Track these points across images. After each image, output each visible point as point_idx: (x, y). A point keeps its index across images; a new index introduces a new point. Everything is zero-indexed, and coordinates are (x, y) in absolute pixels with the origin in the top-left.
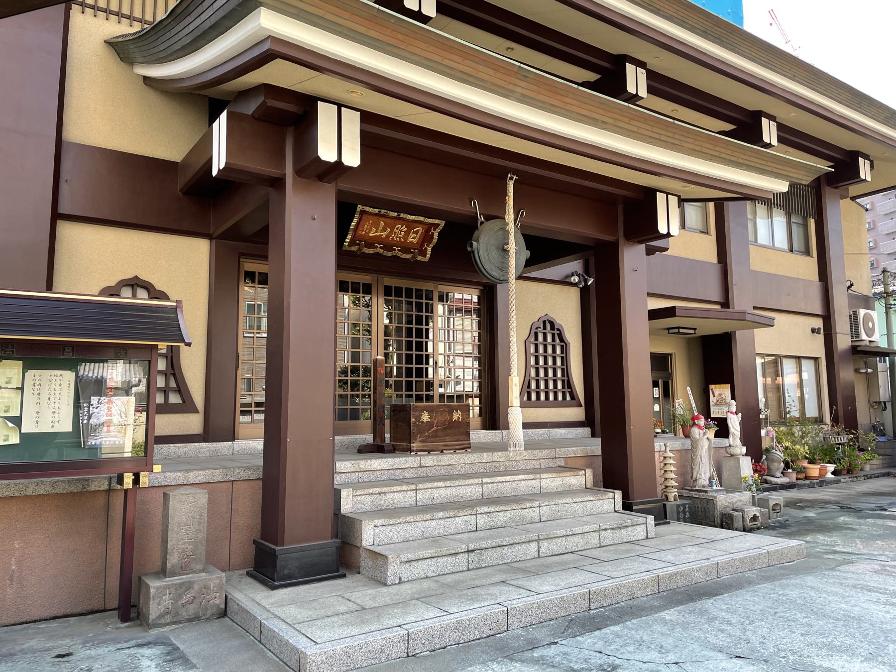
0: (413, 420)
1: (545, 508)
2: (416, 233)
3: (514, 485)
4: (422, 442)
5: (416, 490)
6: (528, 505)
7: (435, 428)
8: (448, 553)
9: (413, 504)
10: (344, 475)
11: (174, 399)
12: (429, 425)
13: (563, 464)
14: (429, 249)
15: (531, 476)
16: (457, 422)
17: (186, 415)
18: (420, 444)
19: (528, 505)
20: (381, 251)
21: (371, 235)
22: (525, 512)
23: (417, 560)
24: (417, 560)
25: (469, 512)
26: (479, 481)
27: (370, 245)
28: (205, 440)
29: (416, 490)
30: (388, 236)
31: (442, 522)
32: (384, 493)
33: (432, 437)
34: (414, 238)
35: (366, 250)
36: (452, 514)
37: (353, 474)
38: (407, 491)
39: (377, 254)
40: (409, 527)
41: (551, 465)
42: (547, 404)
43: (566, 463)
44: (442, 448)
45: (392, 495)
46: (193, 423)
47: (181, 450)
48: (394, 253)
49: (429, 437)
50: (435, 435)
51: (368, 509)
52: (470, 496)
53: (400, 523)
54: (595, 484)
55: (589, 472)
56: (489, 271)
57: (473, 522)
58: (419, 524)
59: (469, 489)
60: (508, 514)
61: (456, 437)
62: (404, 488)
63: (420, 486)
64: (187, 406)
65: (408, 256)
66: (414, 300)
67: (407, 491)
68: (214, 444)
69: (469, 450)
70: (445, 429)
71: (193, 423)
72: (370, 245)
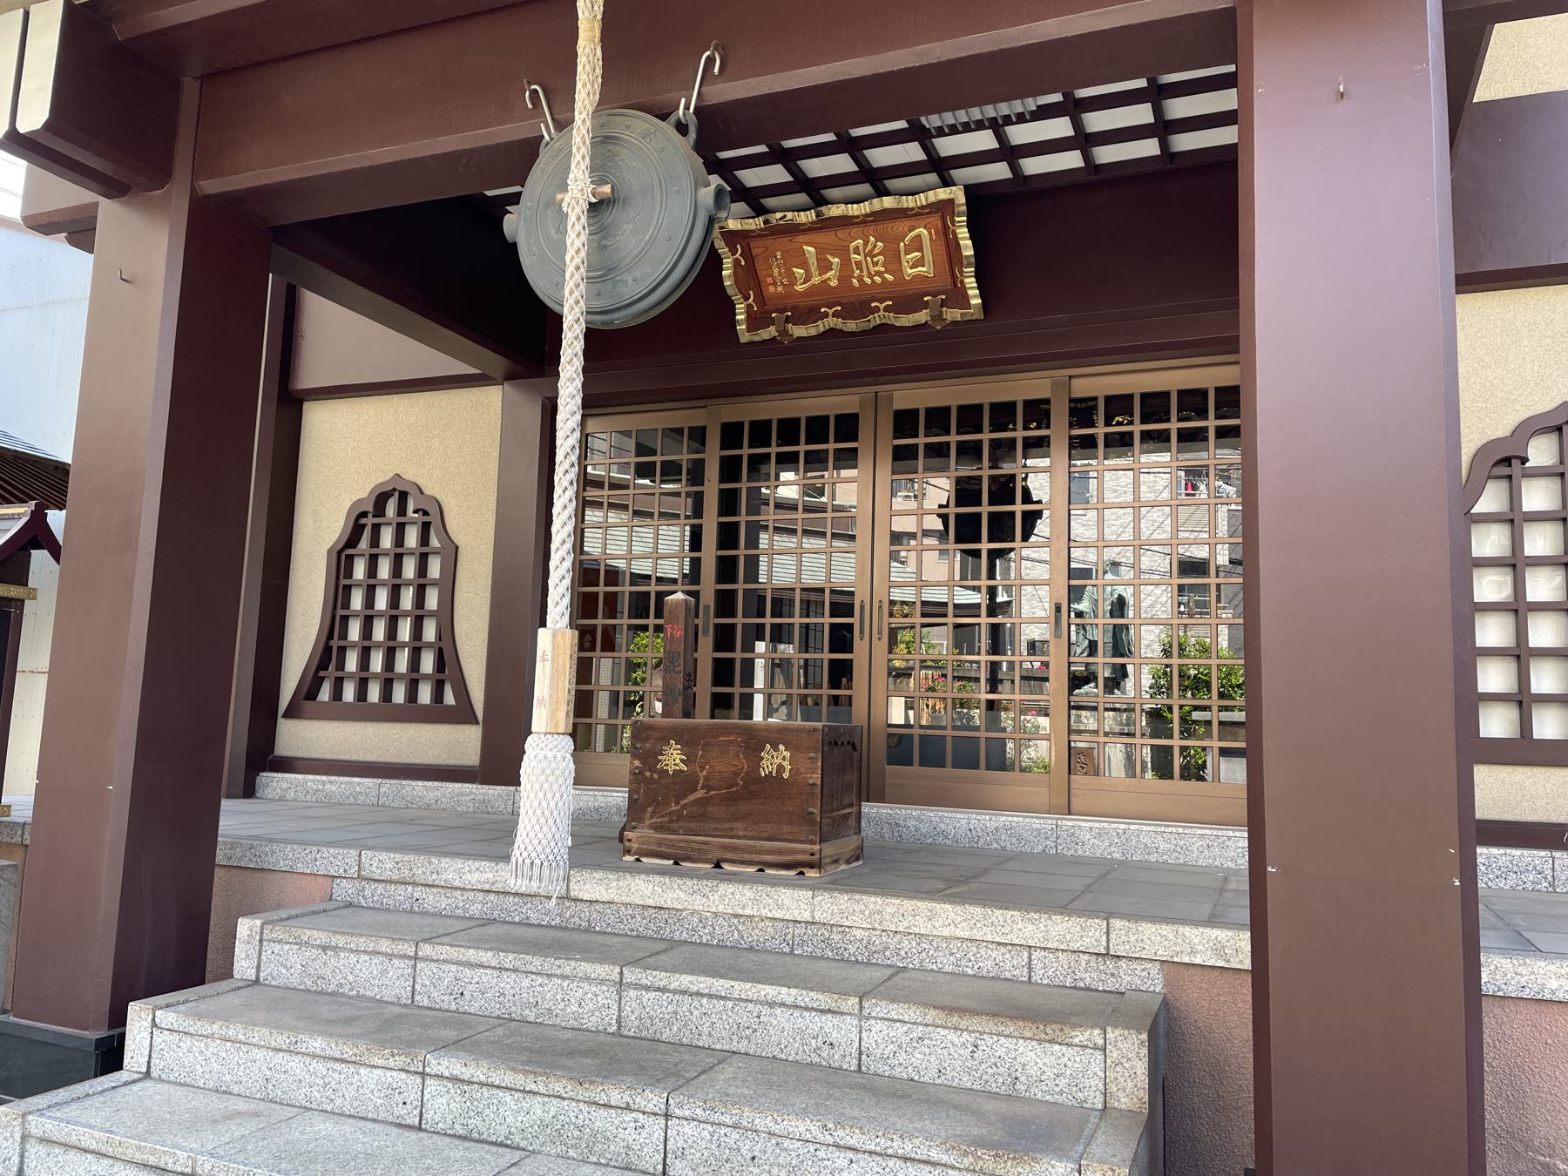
1: (688, 1128)
2: (917, 244)
3: (744, 1015)
4: (658, 828)
5: (416, 958)
6: (616, 1097)
7: (700, 794)
8: (138, 1157)
12: (685, 783)
14: (971, 282)
15: (823, 1000)
16: (775, 780)
18: (651, 834)
19: (616, 1097)
20: (838, 323)
21: (799, 288)
22: (602, 1120)
23: (67, 1146)
24: (67, 1146)
25: (400, 1061)
26: (610, 971)
27: (808, 314)
30: (845, 278)
31: (321, 1067)
32: (335, 949)
33: (692, 817)
35: (799, 331)
36: (348, 1052)
38: (391, 956)
39: (831, 332)
40: (235, 1056)
42: (387, 712)
44: (719, 855)
48: (737, 298)
49: (680, 817)
50: (699, 816)
51: (295, 981)
53: (211, 1036)
57: (413, 1096)
58: (259, 1055)
59: (578, 991)
60: (537, 1107)
61: (768, 828)
62: (385, 945)
63: (426, 950)
64: (462, 713)
65: (922, 316)
67: (391, 956)
69: (811, 874)
70: (732, 799)
71: (464, 744)
72: (808, 314)
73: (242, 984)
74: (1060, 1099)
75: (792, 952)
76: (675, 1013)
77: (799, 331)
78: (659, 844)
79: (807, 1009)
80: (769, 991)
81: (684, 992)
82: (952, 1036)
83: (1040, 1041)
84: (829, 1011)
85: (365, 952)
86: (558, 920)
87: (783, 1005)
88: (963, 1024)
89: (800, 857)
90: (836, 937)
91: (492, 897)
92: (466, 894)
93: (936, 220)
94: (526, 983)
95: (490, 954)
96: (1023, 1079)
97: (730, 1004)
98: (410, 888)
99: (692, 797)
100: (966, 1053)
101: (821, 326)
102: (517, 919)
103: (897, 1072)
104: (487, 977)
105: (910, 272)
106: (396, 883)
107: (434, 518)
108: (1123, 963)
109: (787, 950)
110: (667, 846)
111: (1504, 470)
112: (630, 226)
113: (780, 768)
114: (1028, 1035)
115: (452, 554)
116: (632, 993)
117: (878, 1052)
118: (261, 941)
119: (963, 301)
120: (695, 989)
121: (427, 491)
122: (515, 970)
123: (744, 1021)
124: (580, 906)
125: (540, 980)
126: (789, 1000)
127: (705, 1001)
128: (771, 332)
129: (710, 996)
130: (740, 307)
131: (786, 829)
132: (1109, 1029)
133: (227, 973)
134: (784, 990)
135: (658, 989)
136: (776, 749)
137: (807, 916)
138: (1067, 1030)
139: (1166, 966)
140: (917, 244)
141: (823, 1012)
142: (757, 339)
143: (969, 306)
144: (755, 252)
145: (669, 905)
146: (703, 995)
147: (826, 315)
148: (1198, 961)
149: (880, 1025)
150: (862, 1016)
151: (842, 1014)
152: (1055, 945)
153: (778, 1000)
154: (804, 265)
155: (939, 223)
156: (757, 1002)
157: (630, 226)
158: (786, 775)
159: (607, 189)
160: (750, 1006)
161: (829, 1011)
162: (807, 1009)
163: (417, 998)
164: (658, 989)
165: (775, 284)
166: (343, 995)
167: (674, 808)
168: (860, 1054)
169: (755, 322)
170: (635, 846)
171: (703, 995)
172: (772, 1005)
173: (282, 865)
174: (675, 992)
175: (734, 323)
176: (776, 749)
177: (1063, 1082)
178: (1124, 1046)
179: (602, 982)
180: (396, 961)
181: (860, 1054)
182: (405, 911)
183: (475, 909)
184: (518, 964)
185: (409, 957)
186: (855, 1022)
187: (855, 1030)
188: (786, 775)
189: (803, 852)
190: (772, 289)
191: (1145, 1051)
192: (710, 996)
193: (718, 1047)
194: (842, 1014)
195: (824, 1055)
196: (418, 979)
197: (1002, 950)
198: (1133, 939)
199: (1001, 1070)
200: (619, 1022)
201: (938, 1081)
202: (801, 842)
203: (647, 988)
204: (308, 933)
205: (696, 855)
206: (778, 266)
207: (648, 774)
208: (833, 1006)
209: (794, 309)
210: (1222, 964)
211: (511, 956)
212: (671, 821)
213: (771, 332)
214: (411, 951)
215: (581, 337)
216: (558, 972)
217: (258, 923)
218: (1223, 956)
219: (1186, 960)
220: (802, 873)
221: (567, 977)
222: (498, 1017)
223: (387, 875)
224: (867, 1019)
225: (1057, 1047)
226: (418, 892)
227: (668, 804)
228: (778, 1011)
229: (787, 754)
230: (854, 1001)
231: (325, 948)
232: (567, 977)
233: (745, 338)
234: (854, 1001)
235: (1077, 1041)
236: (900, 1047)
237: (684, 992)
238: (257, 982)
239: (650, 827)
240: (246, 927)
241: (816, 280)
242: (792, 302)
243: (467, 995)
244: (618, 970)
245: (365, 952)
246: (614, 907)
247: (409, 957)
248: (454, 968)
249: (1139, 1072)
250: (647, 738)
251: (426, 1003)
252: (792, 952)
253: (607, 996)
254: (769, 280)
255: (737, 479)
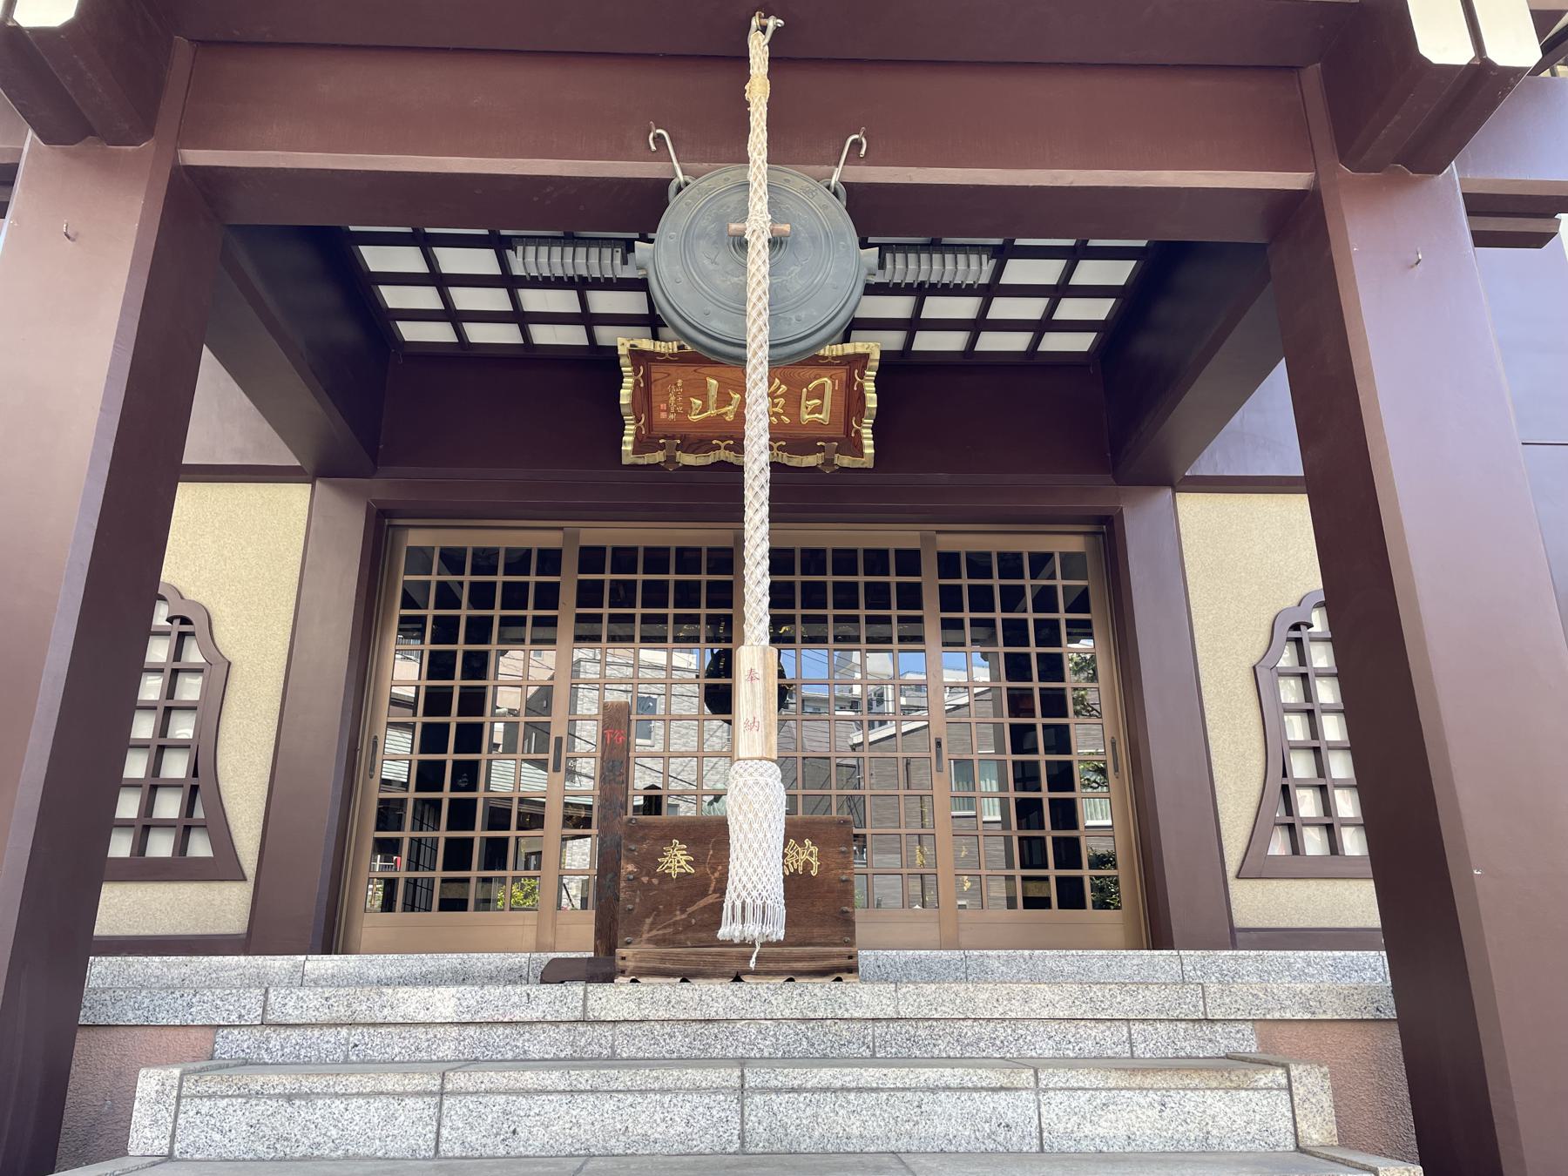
0: (629, 868)
2: (819, 393)
4: (658, 942)
5: (442, 1093)
9: (425, 1146)
10: (295, 1035)
11: (200, 847)
13: (1251, 1047)
14: (867, 433)
17: (216, 886)
18: (651, 948)
21: (694, 418)
28: (246, 951)
29: (442, 1093)
32: (309, 1096)
34: (818, 409)
35: (688, 459)
37: (330, 1034)
38: (400, 1096)
41: (1188, 1048)
43: (1263, 1042)
45: (338, 1105)
46: (225, 906)
47: (175, 972)
48: (629, 419)
49: (688, 927)
51: (237, 1149)
52: (685, 1139)
54: (1346, 1138)
55: (1313, 1084)
56: (696, 318)
59: (682, 1108)
63: (458, 1080)
64: (223, 867)
65: (811, 460)
66: (998, 615)
67: (400, 1096)
68: (259, 959)
71: (225, 906)
73: (139, 1162)
74: (1253, 1147)
75: (873, 1056)
76: (816, 1116)
77: (688, 459)
78: (663, 960)
79: (976, 1089)
80: (929, 1075)
81: (825, 1090)
82: (1138, 1097)
83: (1227, 1090)
84: (1002, 1088)
85: (359, 1094)
86: (569, 1051)
87: (947, 1088)
88: (1148, 1082)
89: (836, 962)
90: (922, 1033)
91: (471, 1030)
92: (431, 1032)
93: (842, 373)
94: (610, 1105)
95: (556, 1075)
96: (1215, 1132)
97: (884, 1096)
98: (344, 1032)
99: (702, 903)
100: (1154, 1113)
101: (711, 458)
102: (510, 1055)
103: (1083, 1146)
104: (549, 1104)
105: (806, 417)
106: (321, 1025)
107: (198, 625)
108: (1218, 1027)
109: (868, 1053)
110: (674, 962)
111: (1295, 634)
112: (798, 269)
113: (807, 864)
114: (1215, 1084)
115: (219, 672)
116: (758, 1099)
117: (1061, 1127)
118: (179, 1098)
119: (858, 450)
120: (838, 1084)
121: (189, 596)
122: (593, 1091)
123: (901, 1114)
124: (599, 1029)
125: (630, 1099)
126: (954, 1083)
127: (852, 1096)
128: (659, 457)
129: (859, 1090)
130: (630, 429)
131: (817, 931)
132: (1292, 1067)
133: (119, 1149)
134: (948, 1071)
135: (793, 1090)
136: (802, 845)
137: (891, 1013)
138: (1250, 1074)
139: (1258, 1025)
140: (819, 393)
141: (994, 1090)
142: (640, 462)
143: (862, 455)
144: (654, 376)
145: (722, 1015)
146: (849, 1090)
147: (718, 447)
148: (1288, 1016)
149: (1060, 1096)
150: (1038, 1090)
151: (1016, 1089)
152: (1155, 1016)
153: (941, 1083)
154: (704, 396)
155: (844, 376)
156: (916, 1089)
157: (798, 269)
158: (814, 872)
159: (786, 228)
160: (909, 1095)
161: (1002, 1088)
162: (976, 1089)
163: (444, 1147)
164: (793, 1090)
165: (668, 411)
166: (321, 1158)
167: (679, 916)
168: (1041, 1132)
169: (641, 446)
170: (630, 964)
171: (849, 1090)
172: (934, 1090)
173: (131, 1018)
174: (813, 1090)
175: (620, 443)
176: (802, 845)
177: (1254, 1128)
178: (1308, 1081)
179: (717, 1091)
180: (410, 1102)
181: (1041, 1132)
182: (335, 1062)
183: (446, 1051)
184: (597, 1082)
185: (431, 1094)
186: (1032, 1097)
187: (1033, 1106)
188: (814, 872)
189: (840, 956)
190: (663, 415)
191: (1327, 1083)
192: (859, 1090)
193: (873, 1149)
194: (1016, 1089)
195: (1000, 1139)
196: (446, 1122)
197: (1101, 1027)
198: (1227, 1000)
199: (1192, 1126)
200: (742, 1137)
201: (1128, 1149)
202: (836, 945)
203: (777, 1091)
204: (261, 1079)
205: (709, 969)
206: (676, 394)
207: (645, 879)
208: (1005, 1082)
209: (684, 438)
210: (1307, 1016)
211: (587, 1075)
212: (677, 933)
213: (659, 457)
214: (434, 1084)
215: (766, 364)
216: (656, 1086)
217: (177, 1072)
218: (1308, 1008)
219: (1277, 1016)
220: (839, 979)
221: (669, 1090)
222: (571, 1155)
223: (310, 1016)
224: (1046, 1090)
225: (1243, 1093)
226: (356, 1035)
227: (671, 912)
228: (942, 1096)
229: (815, 849)
230: (1028, 1074)
231: (290, 1098)
232: (669, 1090)
233: (626, 460)
234: (1028, 1074)
235: (1261, 1084)
236: (1084, 1117)
237: (825, 1090)
238: (170, 1157)
239: (649, 941)
240: (148, 1082)
241: (712, 412)
242: (684, 431)
243: (523, 1134)
244: (737, 1073)
245: (359, 1094)
246: (646, 1026)
247: (431, 1094)
248: (501, 1099)
249: (1326, 1105)
250: (644, 839)
251: (458, 1151)
252: (873, 1056)
253: (724, 1107)
254: (663, 406)
255: (486, 639)
